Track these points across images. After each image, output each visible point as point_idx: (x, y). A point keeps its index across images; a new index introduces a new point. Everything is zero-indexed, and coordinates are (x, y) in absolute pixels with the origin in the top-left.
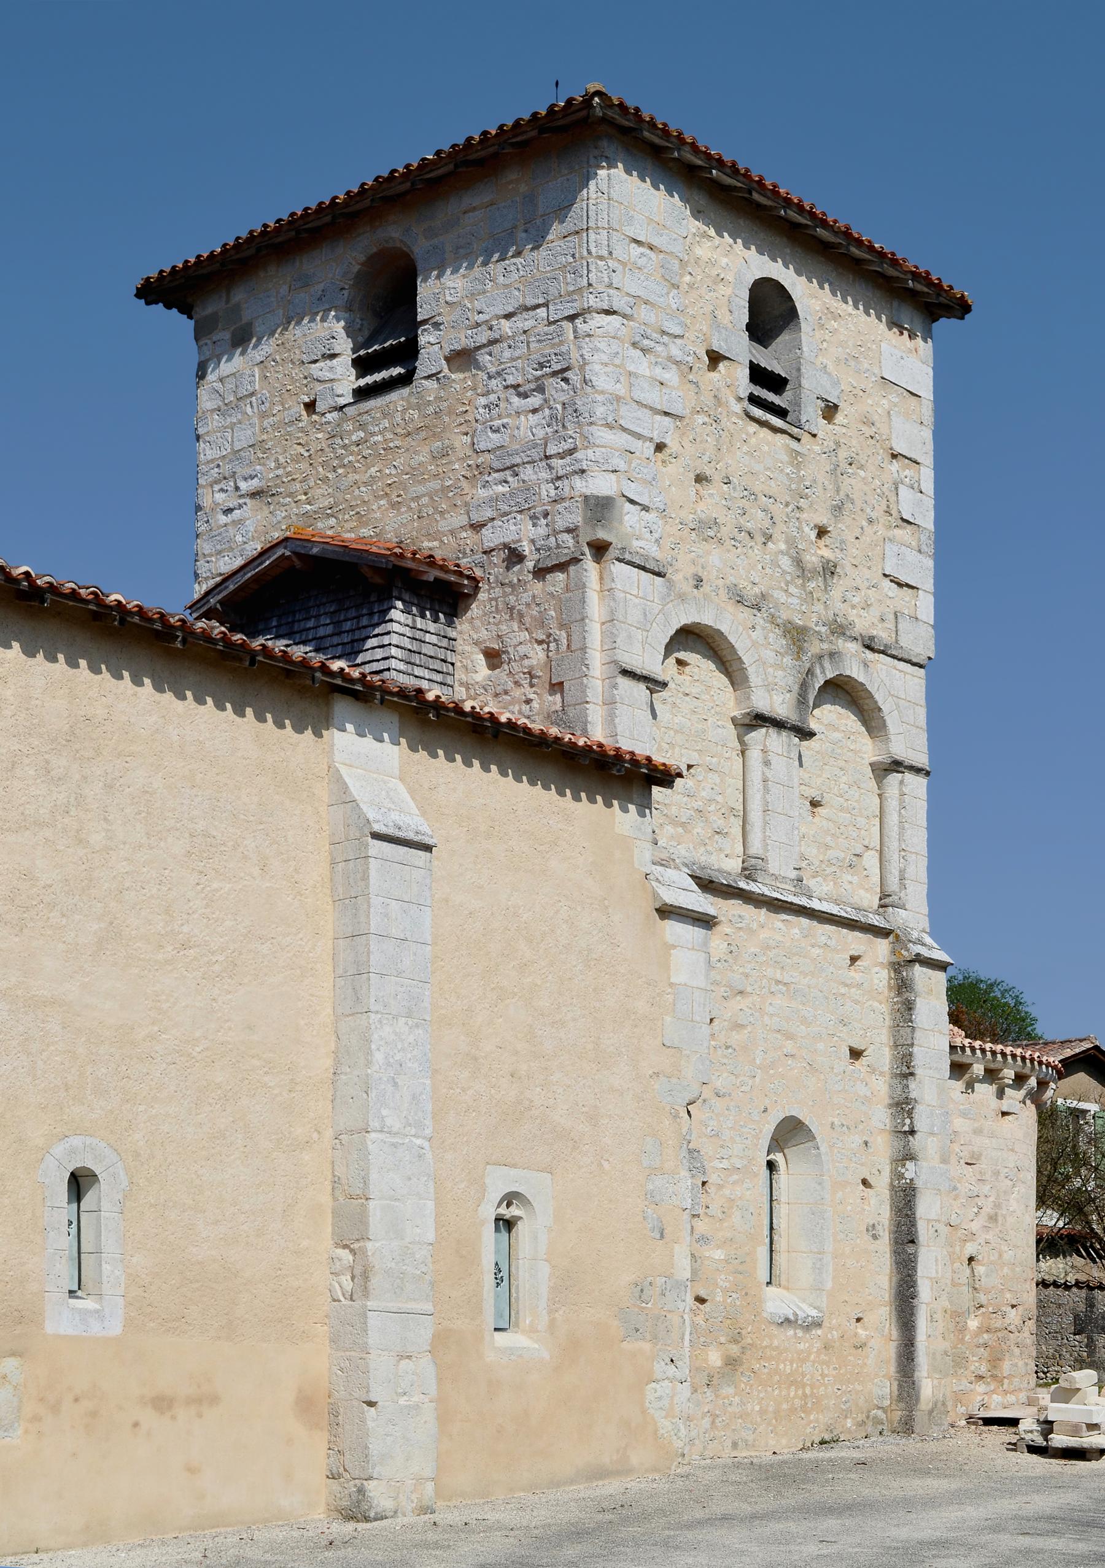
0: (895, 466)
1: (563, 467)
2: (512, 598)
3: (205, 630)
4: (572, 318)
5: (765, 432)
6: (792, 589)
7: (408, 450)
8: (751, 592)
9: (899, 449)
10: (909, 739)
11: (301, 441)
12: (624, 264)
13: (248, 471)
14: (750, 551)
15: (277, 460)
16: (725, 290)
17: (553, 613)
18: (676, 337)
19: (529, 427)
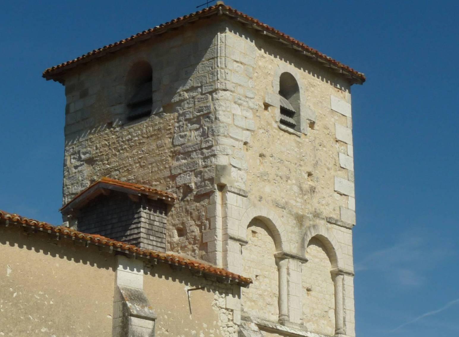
0: (337, 145)
1: (208, 153)
2: (188, 207)
3: (68, 233)
4: (211, 93)
5: (286, 135)
6: (298, 200)
7: (148, 144)
8: (282, 202)
9: (339, 138)
10: (346, 260)
11: (106, 138)
12: (231, 70)
13: (84, 150)
14: (281, 184)
15: (96, 147)
16: (270, 78)
17: (204, 213)
18: (251, 98)
19: (193, 136)
